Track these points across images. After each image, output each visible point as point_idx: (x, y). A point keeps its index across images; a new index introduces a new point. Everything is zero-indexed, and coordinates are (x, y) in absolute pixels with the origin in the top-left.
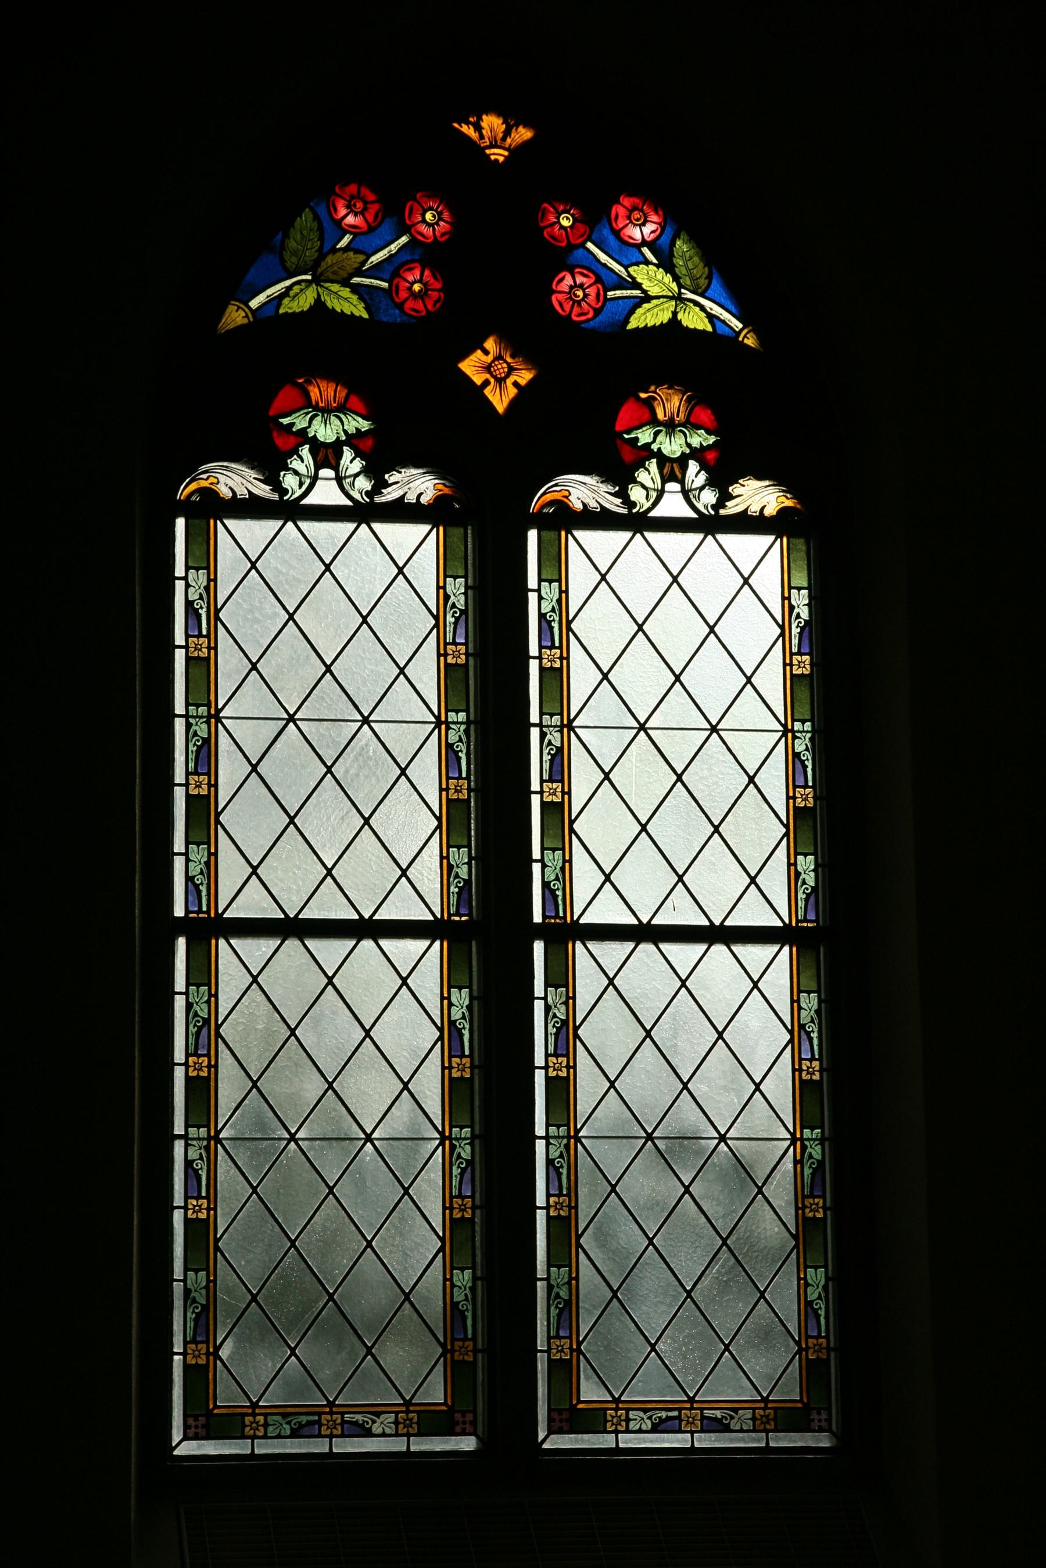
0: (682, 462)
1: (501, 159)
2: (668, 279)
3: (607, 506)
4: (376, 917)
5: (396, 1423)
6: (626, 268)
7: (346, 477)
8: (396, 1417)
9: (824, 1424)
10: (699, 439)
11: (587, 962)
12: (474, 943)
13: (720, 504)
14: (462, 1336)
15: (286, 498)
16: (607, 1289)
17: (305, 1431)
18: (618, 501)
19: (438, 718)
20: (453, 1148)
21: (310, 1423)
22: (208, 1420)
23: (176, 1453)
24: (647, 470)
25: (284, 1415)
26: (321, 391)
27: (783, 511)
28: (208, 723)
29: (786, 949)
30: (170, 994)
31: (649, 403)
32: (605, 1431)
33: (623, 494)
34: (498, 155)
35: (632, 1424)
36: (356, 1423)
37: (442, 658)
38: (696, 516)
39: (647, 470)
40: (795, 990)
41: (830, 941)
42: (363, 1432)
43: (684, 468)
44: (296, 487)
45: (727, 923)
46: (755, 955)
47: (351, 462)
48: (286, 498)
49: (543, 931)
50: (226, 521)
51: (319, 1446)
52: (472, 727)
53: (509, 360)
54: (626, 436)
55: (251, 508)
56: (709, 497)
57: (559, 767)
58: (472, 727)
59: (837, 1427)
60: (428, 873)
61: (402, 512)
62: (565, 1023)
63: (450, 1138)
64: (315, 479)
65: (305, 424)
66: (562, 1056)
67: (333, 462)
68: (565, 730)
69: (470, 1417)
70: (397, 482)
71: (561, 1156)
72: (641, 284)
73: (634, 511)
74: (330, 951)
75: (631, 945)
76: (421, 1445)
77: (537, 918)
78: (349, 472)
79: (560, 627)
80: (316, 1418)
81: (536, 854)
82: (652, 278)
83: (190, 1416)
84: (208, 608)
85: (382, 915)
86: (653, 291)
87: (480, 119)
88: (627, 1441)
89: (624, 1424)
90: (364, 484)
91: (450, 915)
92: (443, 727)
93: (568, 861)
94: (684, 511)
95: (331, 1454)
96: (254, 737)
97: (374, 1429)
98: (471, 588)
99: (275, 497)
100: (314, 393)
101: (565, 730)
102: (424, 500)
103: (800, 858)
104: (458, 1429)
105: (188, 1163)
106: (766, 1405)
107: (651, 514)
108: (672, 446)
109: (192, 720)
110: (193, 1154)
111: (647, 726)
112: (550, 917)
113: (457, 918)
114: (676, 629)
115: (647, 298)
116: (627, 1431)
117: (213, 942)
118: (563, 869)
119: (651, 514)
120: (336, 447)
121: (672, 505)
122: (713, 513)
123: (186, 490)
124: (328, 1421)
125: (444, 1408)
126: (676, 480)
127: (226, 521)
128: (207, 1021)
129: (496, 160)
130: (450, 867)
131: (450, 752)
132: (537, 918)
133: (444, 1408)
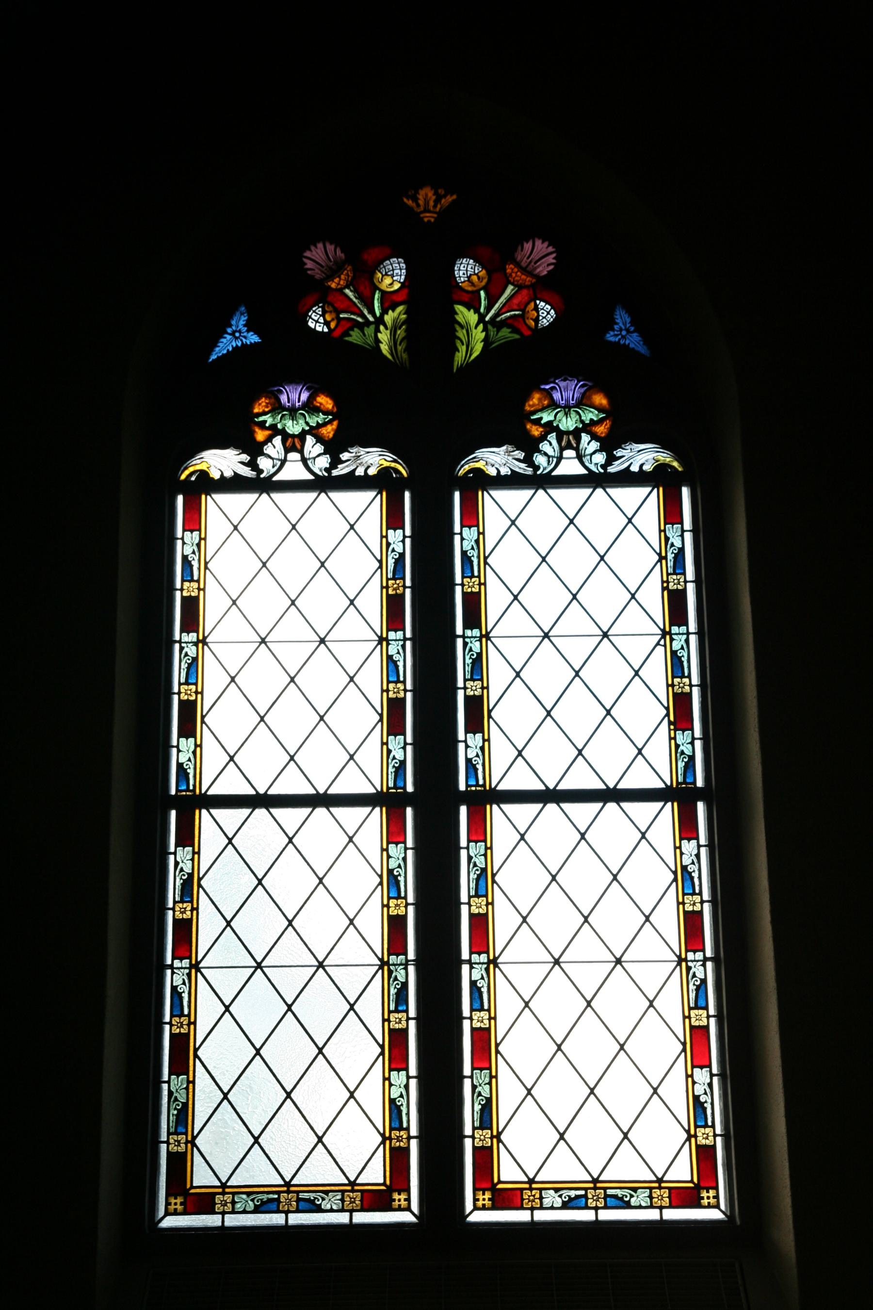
0: (302, 436)
1: (432, 220)
3: (517, 470)
7: (585, 456)
8: (651, 1193)
9: (712, 1201)
11: (502, 821)
14: (703, 1124)
16: (219, 1092)
18: (523, 465)
20: (689, 969)
21: (270, 1201)
28: (481, 641)
31: (548, 394)
32: (214, 1213)
33: (528, 460)
34: (428, 217)
37: (384, 590)
38: (313, 478)
41: (711, 799)
42: (314, 1208)
43: (578, 440)
45: (269, 793)
46: (351, 816)
47: (588, 444)
50: (491, 492)
55: (234, 484)
56: (600, 458)
59: (726, 1206)
62: (191, 875)
64: (560, 458)
65: (551, 418)
66: (482, 896)
67: (299, 447)
70: (623, 456)
73: (539, 472)
74: (291, 816)
77: (462, 787)
78: (312, 455)
80: (276, 1196)
84: (479, 557)
87: (417, 192)
90: (600, 458)
91: (388, 788)
92: (384, 643)
94: (303, 475)
95: (223, 1227)
99: (530, 471)
100: (284, 398)
106: (595, 1185)
107: (553, 474)
108: (294, 427)
109: (467, 640)
110: (476, 975)
116: (233, 1212)
118: (194, 753)
122: (602, 471)
123: (464, 468)
124: (534, 1196)
127: (491, 492)
128: (484, 870)
129: (429, 221)
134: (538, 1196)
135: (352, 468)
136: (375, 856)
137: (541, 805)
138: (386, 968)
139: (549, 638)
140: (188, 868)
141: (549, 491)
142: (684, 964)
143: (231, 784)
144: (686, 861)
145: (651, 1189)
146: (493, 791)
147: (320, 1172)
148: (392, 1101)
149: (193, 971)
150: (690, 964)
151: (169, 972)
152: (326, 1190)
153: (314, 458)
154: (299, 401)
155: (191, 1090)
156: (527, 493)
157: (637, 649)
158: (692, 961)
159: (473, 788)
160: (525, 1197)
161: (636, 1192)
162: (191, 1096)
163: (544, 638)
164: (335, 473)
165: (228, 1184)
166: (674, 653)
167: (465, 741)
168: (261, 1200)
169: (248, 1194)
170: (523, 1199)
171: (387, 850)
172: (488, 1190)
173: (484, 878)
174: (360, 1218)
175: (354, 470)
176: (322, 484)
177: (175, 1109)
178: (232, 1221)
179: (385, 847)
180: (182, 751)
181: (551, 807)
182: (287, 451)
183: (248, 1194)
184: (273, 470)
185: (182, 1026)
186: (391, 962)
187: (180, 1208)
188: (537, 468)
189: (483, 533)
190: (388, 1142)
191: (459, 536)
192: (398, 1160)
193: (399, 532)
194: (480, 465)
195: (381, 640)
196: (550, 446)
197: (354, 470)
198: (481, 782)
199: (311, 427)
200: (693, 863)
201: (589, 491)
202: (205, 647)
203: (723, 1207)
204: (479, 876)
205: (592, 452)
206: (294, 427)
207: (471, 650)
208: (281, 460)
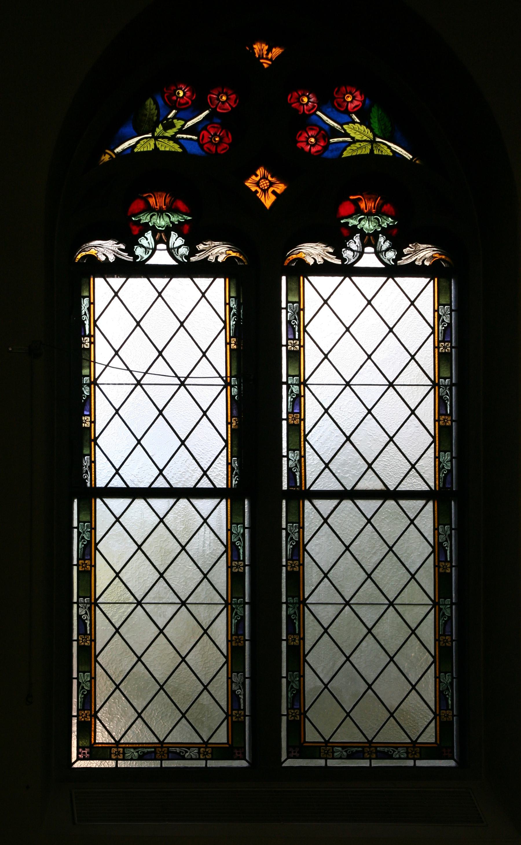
0: (167, 232)
2: (367, 131)
3: (329, 260)
4: (110, 486)
5: (199, 753)
6: (341, 125)
9: (240, 755)
12: (246, 502)
15: (345, 263)
22: (90, 750)
23: (284, 765)
27: (230, 259)
29: (224, 502)
31: (356, 202)
36: (176, 753)
38: (384, 266)
40: (229, 523)
44: (351, 257)
46: (412, 506)
47: (176, 240)
48: (345, 263)
49: (287, 495)
51: (365, 763)
53: (269, 178)
54: (133, 219)
55: (325, 269)
56: (391, 255)
59: (249, 757)
60: (427, 466)
63: (231, 604)
64: (154, 250)
68: (302, 386)
71: (295, 613)
72: (349, 134)
73: (138, 260)
75: (129, 501)
77: (285, 487)
81: (284, 452)
82: (357, 131)
86: (358, 137)
88: (332, 763)
90: (391, 255)
93: (303, 457)
94: (169, 261)
97: (186, 756)
98: (454, 311)
100: (152, 201)
101: (302, 386)
102: (220, 260)
103: (442, 453)
105: (79, 617)
106: (162, 745)
107: (356, 265)
108: (368, 226)
111: (351, 383)
112: (291, 487)
114: (370, 330)
115: (354, 141)
117: (93, 500)
119: (356, 265)
120: (375, 235)
121: (370, 260)
125: (227, 746)
131: (441, 400)
132: (285, 487)
133: (227, 746)
135: (413, 259)
144: (442, 538)
147: (392, 735)
152: (189, 746)
154: (366, 209)
156: (338, 279)
158: (442, 605)
161: (397, 749)
164: (193, 259)
165: (165, 741)
168: (352, 751)
169: (135, 748)
170: (320, 752)
172: (87, 747)
174: (212, 764)
175: (208, 257)
176: (390, 271)
182: (157, 243)
186: (441, 603)
187: (297, 755)
188: (344, 260)
190: (230, 718)
192: (235, 728)
194: (93, 252)
196: (355, 243)
197: (208, 257)
199: (383, 228)
200: (446, 541)
206: (368, 226)
208: (359, 252)
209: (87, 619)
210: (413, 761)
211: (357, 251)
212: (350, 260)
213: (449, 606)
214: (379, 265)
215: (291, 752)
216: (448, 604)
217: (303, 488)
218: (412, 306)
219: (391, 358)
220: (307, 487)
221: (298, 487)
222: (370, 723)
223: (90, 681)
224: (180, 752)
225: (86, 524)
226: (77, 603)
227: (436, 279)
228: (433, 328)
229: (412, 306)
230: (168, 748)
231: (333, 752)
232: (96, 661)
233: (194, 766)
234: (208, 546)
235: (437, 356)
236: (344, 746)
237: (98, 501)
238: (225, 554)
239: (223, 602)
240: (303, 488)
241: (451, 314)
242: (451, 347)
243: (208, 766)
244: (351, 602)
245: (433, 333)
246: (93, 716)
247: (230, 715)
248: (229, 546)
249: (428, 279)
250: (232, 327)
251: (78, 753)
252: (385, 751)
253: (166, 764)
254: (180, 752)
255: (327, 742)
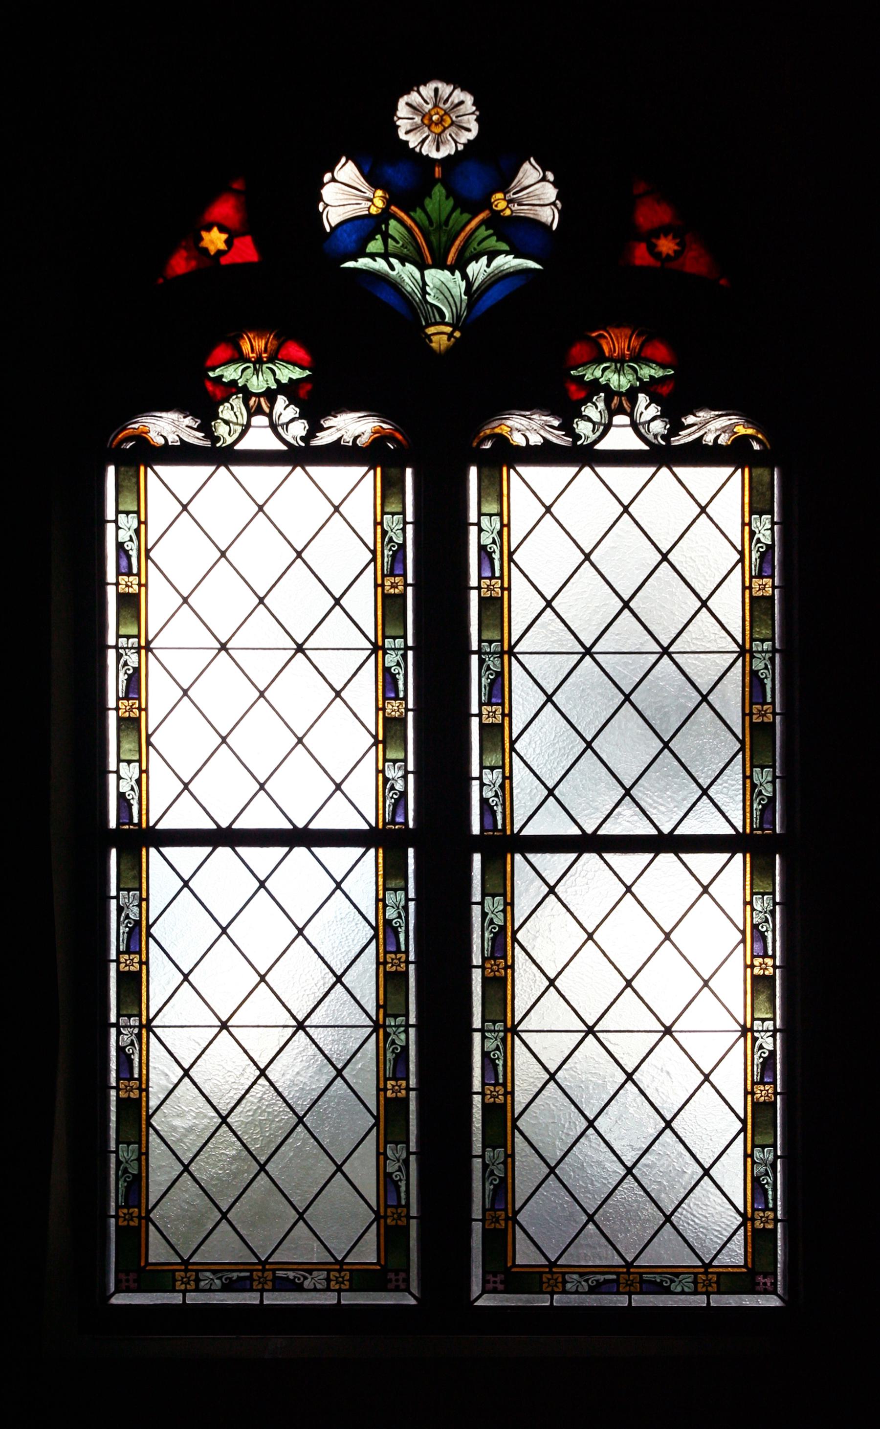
0: (632, 395)
3: (555, 440)
5: (328, 1280)
8: (328, 1275)
10: (287, 373)
13: (311, 434)
15: (218, 445)
17: (604, 1288)
19: (742, 647)
20: (754, 1040)
24: (594, 404)
25: (214, 1272)
26: (616, 342)
30: (468, 904)
33: (567, 428)
35: (568, 1286)
38: (647, 448)
39: (594, 404)
43: (633, 402)
45: (311, 827)
46: (339, 858)
47: (646, 408)
48: (218, 445)
51: (250, 1298)
52: (777, 656)
55: (545, 455)
56: (299, 429)
57: (498, 690)
58: (777, 656)
59: (784, 1289)
60: (363, 788)
61: (340, 454)
63: (384, 1026)
64: (608, 427)
68: (506, 657)
69: (402, 1275)
73: (579, 443)
74: (629, 864)
76: (349, 1299)
77: (476, 829)
79: (500, 558)
83: (489, 1273)
85: (683, 830)
89: (560, 1285)
92: (380, 653)
93: (508, 778)
94: (633, 443)
96: (550, 671)
98: (777, 523)
99: (207, 443)
100: (246, 347)
104: (390, 1286)
107: (236, 448)
108: (620, 381)
110: (125, 1040)
111: (593, 650)
112: (125, 824)
113: (759, 832)
117: (509, 856)
121: (621, 438)
122: (303, 444)
124: (343, 1277)
125: (744, 1270)
126: (262, 413)
130: (754, 786)
131: (387, 674)
132: (476, 829)
134: (560, 1279)
136: (736, 911)
137: (287, 849)
138: (749, 1034)
139: (227, 650)
140: (499, 920)
141: (231, 468)
142: (749, 1034)
143: (551, 823)
144: (391, 913)
145: (696, 1274)
146: (151, 830)
147: (302, 1249)
148: (756, 1180)
149: (509, 1035)
150: (756, 1034)
151: (113, 1031)
152: (309, 1268)
153: (287, 424)
154: (253, 352)
155: (143, 1163)
157: (338, 667)
159: (127, 827)
160: (545, 1280)
161: (311, 1274)
162: (144, 1168)
163: (220, 650)
166: (387, 670)
167: (117, 772)
171: (751, 903)
173: (138, 934)
176: (298, 456)
177: (491, 1183)
178: (193, 1298)
179: (748, 899)
180: (120, 780)
181: (300, 852)
183: (581, 1275)
184: (593, 437)
185: (132, 1090)
186: (755, 1028)
189: (145, 523)
191: (113, 525)
192: (392, 1238)
193: (766, 518)
195: (376, 648)
196: (594, 411)
198: (136, 820)
201: (574, 470)
202: (150, 653)
203: (415, 1291)
204: (131, 930)
205: (649, 418)
206: (620, 381)
207: (126, 664)
209: (498, 1058)
210: (548, 1296)
211: (600, 424)
212: (587, 438)
213: (402, 1029)
214: (639, 445)
215: (488, 1282)
216: (769, 1031)
217: (508, 832)
218: (625, 515)
219: (300, 603)
220: (516, 831)
221: (500, 831)
222: (265, 1231)
223: (139, 1160)
224: (295, 1277)
225: (131, 893)
226: (482, 1030)
227: (747, 470)
228: (374, 552)
229: (625, 515)
230: (641, 1274)
231: (565, 1282)
232: (149, 1125)
233: (159, 1302)
234: (345, 932)
235: (747, 600)
236: (217, 1269)
237: (518, 857)
238: (374, 941)
239: (372, 1024)
240: (508, 832)
241: (772, 529)
242: (774, 587)
243: (633, 1305)
244: (307, 1023)
245: (742, 560)
246: (749, 1219)
247: (749, 1219)
248: (381, 928)
249: (366, 468)
250: (386, 560)
251: (485, 1281)
252: (659, 1280)
253: (639, 1300)
254: (295, 1277)
255: (552, 1264)
